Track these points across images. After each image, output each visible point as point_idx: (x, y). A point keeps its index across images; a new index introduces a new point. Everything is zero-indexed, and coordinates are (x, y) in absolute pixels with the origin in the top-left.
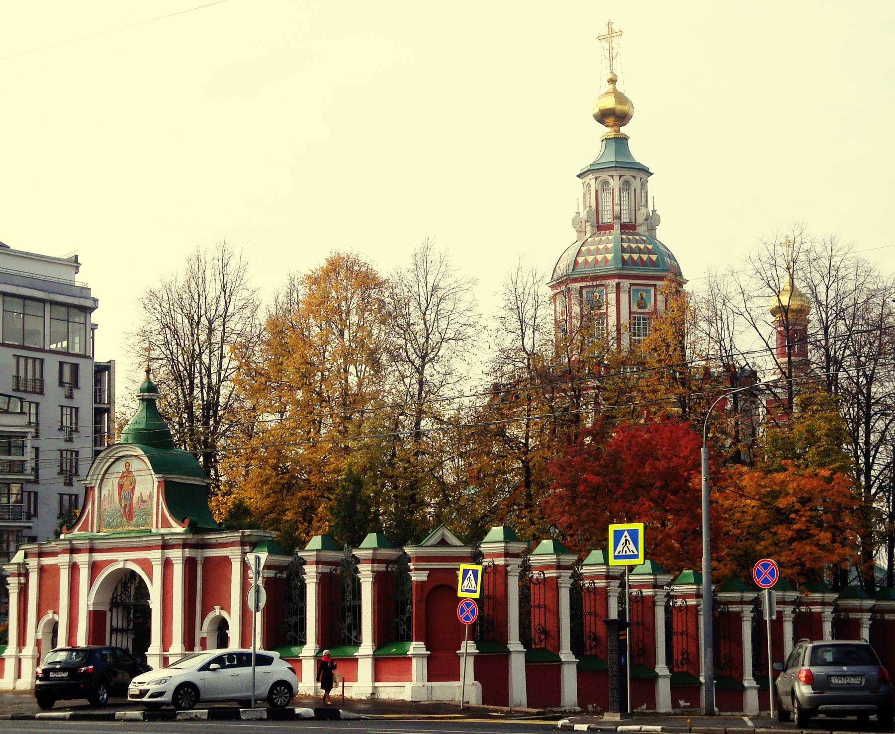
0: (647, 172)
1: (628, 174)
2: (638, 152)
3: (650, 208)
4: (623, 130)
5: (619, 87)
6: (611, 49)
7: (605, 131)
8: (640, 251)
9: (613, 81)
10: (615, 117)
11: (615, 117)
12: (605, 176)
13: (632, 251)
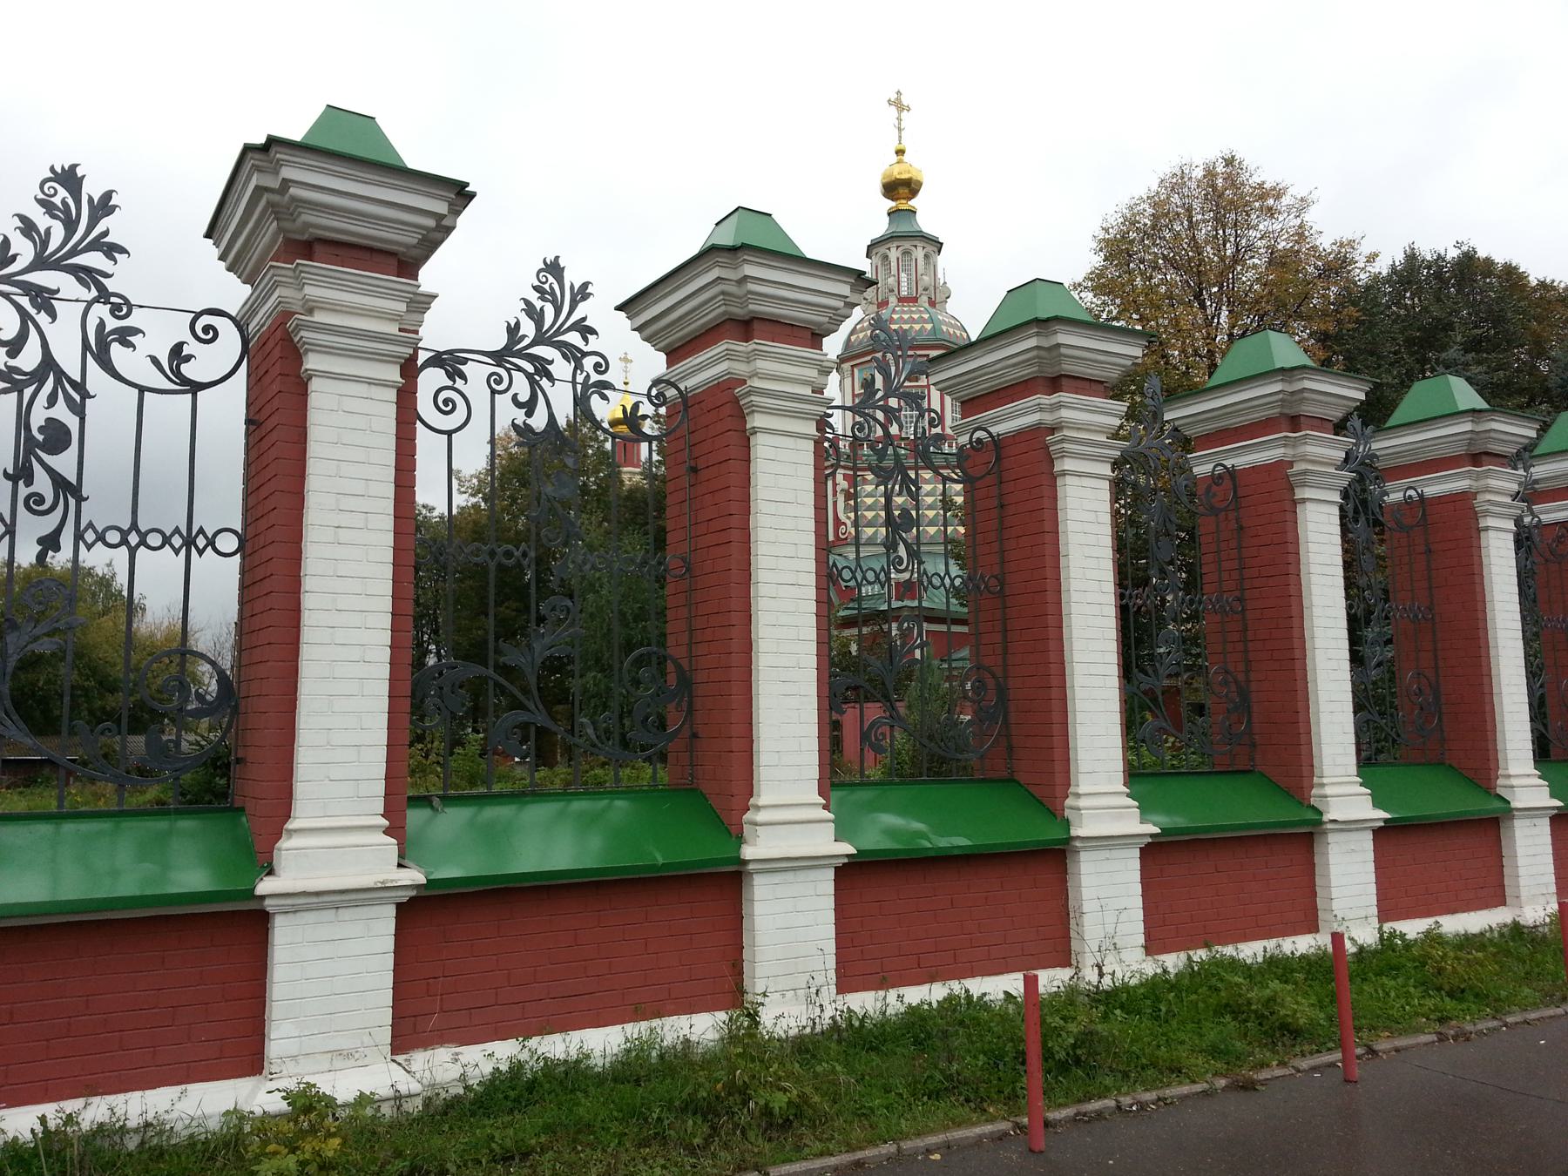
0: (939, 246)
1: (907, 245)
2: (926, 222)
3: (940, 275)
4: (913, 203)
5: (906, 158)
6: (899, 119)
7: (891, 204)
8: (913, 321)
9: (900, 152)
10: (900, 189)
11: (900, 189)
12: (882, 250)
13: (913, 321)
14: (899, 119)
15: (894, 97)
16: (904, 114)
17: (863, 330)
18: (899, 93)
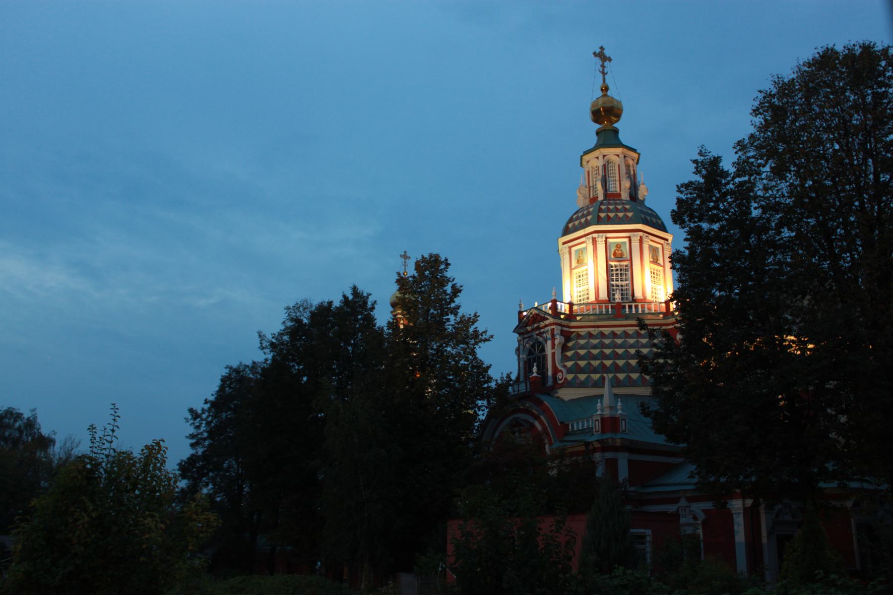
4: (615, 125)
6: (603, 66)
14: (603, 66)
15: (598, 50)
16: (606, 64)
17: (577, 219)
18: (602, 48)
